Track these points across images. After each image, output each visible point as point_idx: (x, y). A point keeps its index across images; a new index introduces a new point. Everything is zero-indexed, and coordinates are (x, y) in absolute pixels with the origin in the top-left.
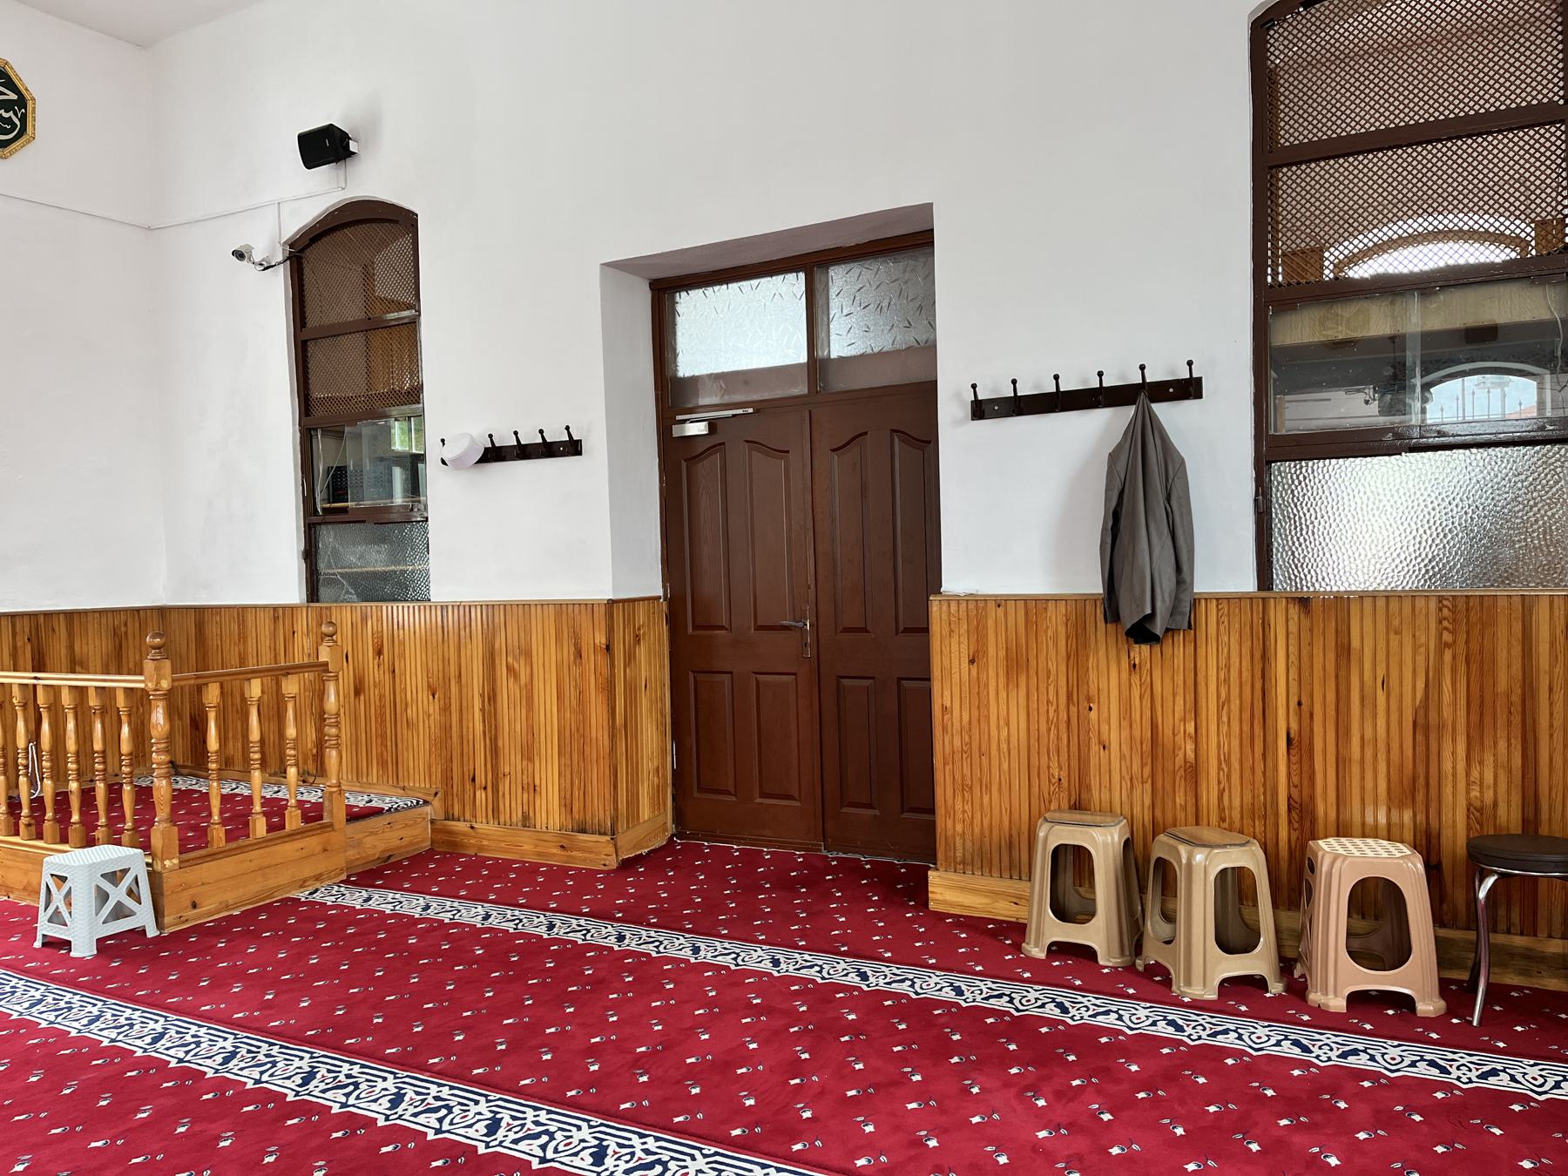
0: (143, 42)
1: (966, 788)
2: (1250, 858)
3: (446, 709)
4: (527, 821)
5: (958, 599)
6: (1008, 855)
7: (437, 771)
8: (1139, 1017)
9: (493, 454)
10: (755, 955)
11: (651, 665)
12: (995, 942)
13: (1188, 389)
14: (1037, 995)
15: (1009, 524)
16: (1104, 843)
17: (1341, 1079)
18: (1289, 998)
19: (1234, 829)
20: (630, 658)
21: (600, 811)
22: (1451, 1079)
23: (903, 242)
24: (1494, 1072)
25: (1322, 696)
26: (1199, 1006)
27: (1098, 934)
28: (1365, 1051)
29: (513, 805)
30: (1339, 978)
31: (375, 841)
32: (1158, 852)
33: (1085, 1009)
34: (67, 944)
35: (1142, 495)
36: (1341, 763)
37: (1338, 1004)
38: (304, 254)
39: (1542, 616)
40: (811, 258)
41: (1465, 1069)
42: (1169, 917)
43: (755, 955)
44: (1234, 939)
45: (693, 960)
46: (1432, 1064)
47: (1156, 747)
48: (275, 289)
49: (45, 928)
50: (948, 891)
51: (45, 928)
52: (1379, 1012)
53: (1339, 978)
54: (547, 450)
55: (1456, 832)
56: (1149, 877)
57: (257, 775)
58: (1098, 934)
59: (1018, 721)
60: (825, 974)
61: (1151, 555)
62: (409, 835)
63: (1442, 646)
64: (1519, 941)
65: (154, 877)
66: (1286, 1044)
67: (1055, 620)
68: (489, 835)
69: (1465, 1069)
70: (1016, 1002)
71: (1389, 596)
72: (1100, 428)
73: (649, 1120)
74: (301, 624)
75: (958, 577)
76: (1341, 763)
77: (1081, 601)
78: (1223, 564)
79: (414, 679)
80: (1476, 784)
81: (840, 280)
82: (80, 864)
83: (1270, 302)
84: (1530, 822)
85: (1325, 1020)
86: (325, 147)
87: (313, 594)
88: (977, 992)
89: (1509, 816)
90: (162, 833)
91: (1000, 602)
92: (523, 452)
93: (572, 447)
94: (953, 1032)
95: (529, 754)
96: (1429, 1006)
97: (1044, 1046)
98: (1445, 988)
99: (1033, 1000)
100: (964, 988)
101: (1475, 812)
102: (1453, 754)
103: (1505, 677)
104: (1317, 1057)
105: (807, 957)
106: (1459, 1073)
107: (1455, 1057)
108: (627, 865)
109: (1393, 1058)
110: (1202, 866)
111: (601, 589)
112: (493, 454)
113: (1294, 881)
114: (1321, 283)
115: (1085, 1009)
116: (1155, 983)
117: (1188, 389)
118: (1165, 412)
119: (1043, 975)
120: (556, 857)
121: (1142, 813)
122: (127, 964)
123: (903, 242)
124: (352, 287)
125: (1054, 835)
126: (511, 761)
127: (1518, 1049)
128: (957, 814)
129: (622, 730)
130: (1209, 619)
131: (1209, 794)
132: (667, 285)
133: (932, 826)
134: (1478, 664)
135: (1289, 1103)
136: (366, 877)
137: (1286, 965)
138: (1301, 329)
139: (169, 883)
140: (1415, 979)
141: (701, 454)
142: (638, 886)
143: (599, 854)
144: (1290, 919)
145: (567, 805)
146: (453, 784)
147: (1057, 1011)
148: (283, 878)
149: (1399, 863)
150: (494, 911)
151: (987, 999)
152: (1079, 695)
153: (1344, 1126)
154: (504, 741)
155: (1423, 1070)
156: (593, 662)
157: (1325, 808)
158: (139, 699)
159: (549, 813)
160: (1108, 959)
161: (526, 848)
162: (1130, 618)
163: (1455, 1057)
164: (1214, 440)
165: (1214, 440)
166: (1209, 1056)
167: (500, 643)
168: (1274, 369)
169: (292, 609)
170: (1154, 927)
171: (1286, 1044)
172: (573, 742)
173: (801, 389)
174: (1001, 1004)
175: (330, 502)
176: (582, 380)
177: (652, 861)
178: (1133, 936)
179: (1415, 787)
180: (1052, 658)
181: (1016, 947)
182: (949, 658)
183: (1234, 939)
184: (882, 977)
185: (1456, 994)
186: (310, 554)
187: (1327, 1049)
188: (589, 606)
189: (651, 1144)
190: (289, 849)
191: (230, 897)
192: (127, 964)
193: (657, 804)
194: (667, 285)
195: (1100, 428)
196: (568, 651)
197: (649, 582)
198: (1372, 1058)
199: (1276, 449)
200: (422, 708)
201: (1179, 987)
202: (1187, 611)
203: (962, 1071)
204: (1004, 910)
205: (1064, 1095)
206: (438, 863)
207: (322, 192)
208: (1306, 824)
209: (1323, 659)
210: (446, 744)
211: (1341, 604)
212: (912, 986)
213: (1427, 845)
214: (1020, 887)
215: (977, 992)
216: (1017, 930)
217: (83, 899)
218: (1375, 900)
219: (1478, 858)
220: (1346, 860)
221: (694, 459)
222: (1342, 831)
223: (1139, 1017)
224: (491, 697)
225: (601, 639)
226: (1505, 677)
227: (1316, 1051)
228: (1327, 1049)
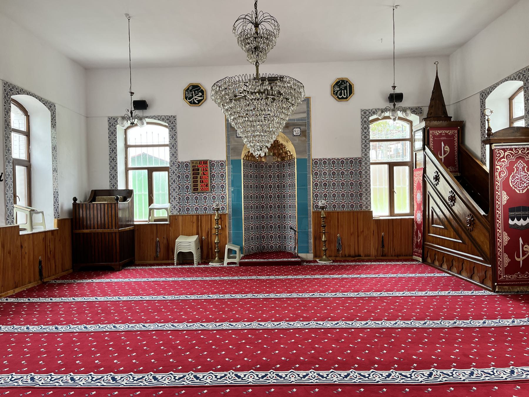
10: (43, 381)
14: (165, 382)
28: (260, 378)
43: (84, 381)
45: (33, 374)
60: (50, 377)
66: (284, 376)
70: (173, 377)
75: (524, 126)
94: (154, 362)
100: (153, 380)
104: (274, 373)
105: (57, 384)
106: (273, 375)
107: (316, 381)
147: (198, 376)
150: (478, 372)
151: (143, 377)
163: (316, 381)
171: (367, 376)
174: (137, 376)
198: (216, 376)
212: (175, 377)
227: (274, 375)
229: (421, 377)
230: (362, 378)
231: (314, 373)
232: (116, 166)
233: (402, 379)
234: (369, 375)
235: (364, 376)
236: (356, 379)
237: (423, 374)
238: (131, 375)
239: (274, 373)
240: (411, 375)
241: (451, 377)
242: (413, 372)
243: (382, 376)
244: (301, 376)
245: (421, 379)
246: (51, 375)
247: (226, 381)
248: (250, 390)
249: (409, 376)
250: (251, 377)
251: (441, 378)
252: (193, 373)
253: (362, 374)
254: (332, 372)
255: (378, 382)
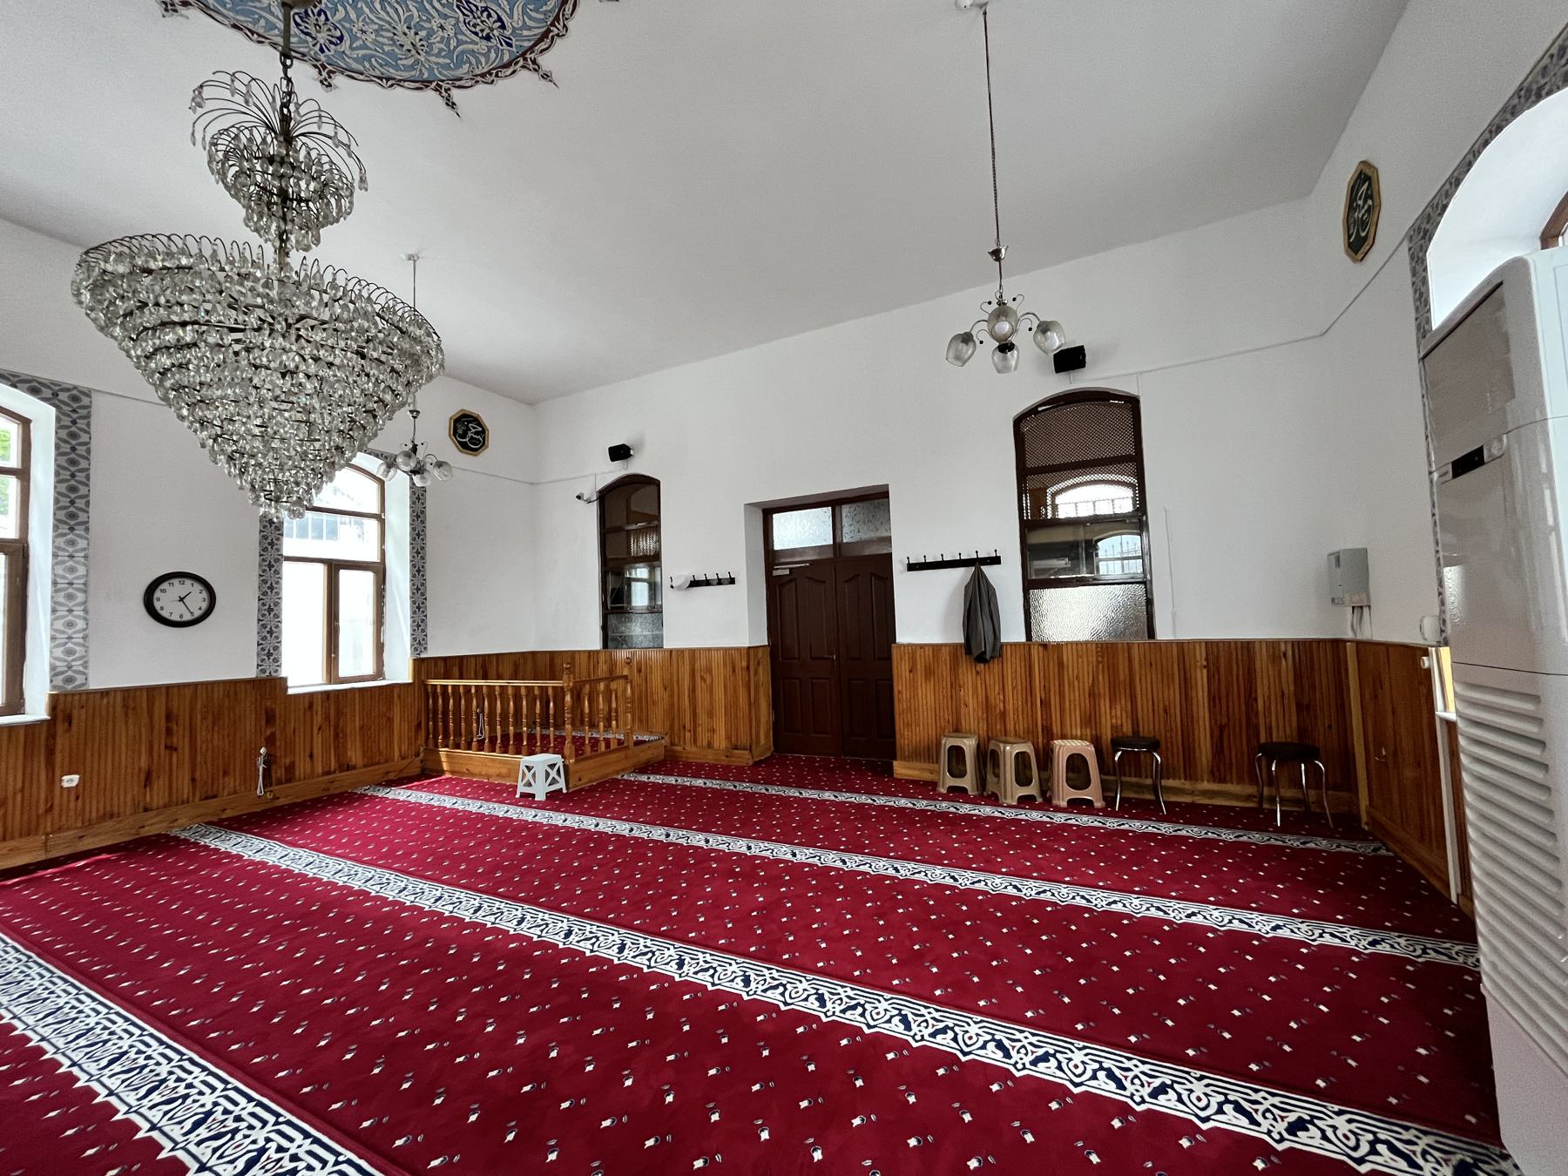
0: (531, 404)
1: (908, 725)
2: (1027, 748)
3: (672, 696)
4: (710, 745)
5: (904, 646)
6: (928, 753)
7: (667, 724)
8: (987, 811)
9: (695, 583)
11: (764, 675)
12: (926, 788)
13: (995, 560)
15: (924, 615)
16: (969, 745)
17: (1065, 827)
18: (1046, 802)
19: (1022, 738)
20: (756, 673)
21: (744, 740)
22: (1170, 917)
23: (875, 499)
24: (1194, 914)
25: (1054, 687)
26: (1010, 806)
27: (967, 782)
28: (1054, 1056)
29: (703, 738)
30: (1065, 794)
31: (644, 755)
32: (991, 747)
33: (965, 809)
34: (533, 796)
35: (979, 602)
36: (1062, 710)
37: (1064, 804)
38: (607, 497)
39: (1135, 650)
40: (834, 502)
41: (1112, 824)
42: (997, 776)
44: (1023, 780)
46: (1158, 909)
47: (988, 706)
48: (593, 511)
49: (521, 789)
50: (901, 769)
51: (521, 789)
52: (1076, 806)
53: (1065, 794)
54: (720, 582)
55: (1107, 735)
56: (988, 758)
57: (568, 727)
58: (967, 782)
59: (930, 697)
61: (984, 626)
62: (659, 753)
63: (1098, 662)
64: (1134, 780)
65: (565, 766)
66: (991, 1046)
67: (945, 653)
68: (689, 751)
69: (1112, 824)
71: (1077, 643)
72: (961, 575)
73: (705, 943)
74: (602, 658)
75: (904, 636)
76: (1062, 710)
77: (955, 646)
78: (1012, 631)
79: (656, 681)
80: (1113, 718)
81: (846, 510)
82: (541, 760)
83: (1027, 527)
84: (1136, 732)
85: (1058, 809)
86: (620, 453)
87: (605, 645)
88: (922, 804)
89: (1127, 729)
90: (568, 747)
91: (922, 646)
92: (707, 583)
93: (732, 581)
95: (711, 715)
96: (1098, 804)
97: (954, 821)
98: (1105, 798)
99: (944, 806)
101: (1114, 728)
102: (1104, 705)
103: (1123, 674)
105: (776, 975)
108: (757, 764)
109: (1085, 820)
110: (1010, 751)
111: (744, 641)
112: (695, 583)
113: (1046, 757)
114: (1046, 520)
115: (965, 809)
116: (993, 800)
117: (995, 560)
118: (987, 570)
119: (945, 798)
120: (724, 761)
121: (983, 733)
122: (555, 800)
123: (875, 499)
124: (628, 511)
125: (948, 742)
126: (702, 718)
127: (1133, 817)
128: (907, 735)
129: (753, 704)
130: (1008, 653)
131: (1010, 726)
132: (768, 512)
133: (894, 743)
134: (1112, 670)
135: (1045, 834)
136: (644, 769)
137: (1043, 793)
138: (1039, 538)
139: (571, 769)
140: (1093, 794)
141: (785, 583)
142: (761, 770)
143: (744, 758)
144: (1045, 775)
145: (728, 738)
146: (674, 729)
148: (610, 770)
149: (1085, 748)
152: (955, 685)
153: (1068, 840)
154: (699, 710)
155: (1153, 913)
156: (740, 677)
157: (1056, 729)
158: (558, 693)
159: (720, 742)
160: (972, 792)
161: (709, 757)
162: (976, 653)
164: (1007, 580)
165: (1007, 580)
166: (1016, 822)
167: (697, 666)
168: (1029, 552)
169: (597, 652)
170: (990, 778)
172: (732, 708)
173: (831, 555)
175: (615, 602)
176: (735, 554)
177: (768, 762)
178: (982, 782)
179: (1091, 719)
180: (944, 670)
181: (934, 789)
182: (900, 669)
183: (1023, 780)
184: (881, 801)
185: (1110, 801)
186: (604, 628)
187: (1060, 818)
188: (739, 649)
189: (708, 958)
190: (613, 757)
191: (593, 776)
192: (555, 800)
193: (767, 737)
194: (768, 512)
195: (961, 575)
196: (729, 669)
197: (763, 640)
199: (1032, 584)
200: (659, 693)
201: (1002, 799)
202: (999, 649)
203: (922, 828)
204: (926, 776)
205: (961, 834)
206: (669, 763)
207: (617, 471)
208: (1049, 735)
209: (1053, 669)
210: (672, 712)
211: (1059, 646)
213: (1096, 742)
214: (935, 766)
215: (922, 804)
216: (934, 785)
217: (541, 776)
218: (1076, 764)
219: (1116, 744)
220: (1065, 748)
221: (781, 586)
222: (1063, 737)
223: (987, 811)
224: (693, 690)
225: (744, 664)
226: (1123, 674)
228: (1060, 818)
229: (1335, 1128)
230: (1246, 1105)
231: (1132, 1097)
232: (413, 503)
233: (1128, 1070)
234: (1220, 1111)
235: (1239, 1108)
236: (1136, 1071)
237: (1325, 1137)
238: (786, 1004)
239: (1015, 1065)
240: (1094, 1077)
241: (1383, 1135)
242: (1205, 1120)
243: (1323, 1131)
244: (1172, 1095)
245: (1340, 1121)
246: (713, 984)
247: (937, 1015)
248: (896, 982)
249: (1228, 1108)
250: (1076, 1067)
251: (1267, 1105)
252: (1012, 1068)
253: (1244, 1121)
254: (1076, 1085)
255: (1200, 1079)
